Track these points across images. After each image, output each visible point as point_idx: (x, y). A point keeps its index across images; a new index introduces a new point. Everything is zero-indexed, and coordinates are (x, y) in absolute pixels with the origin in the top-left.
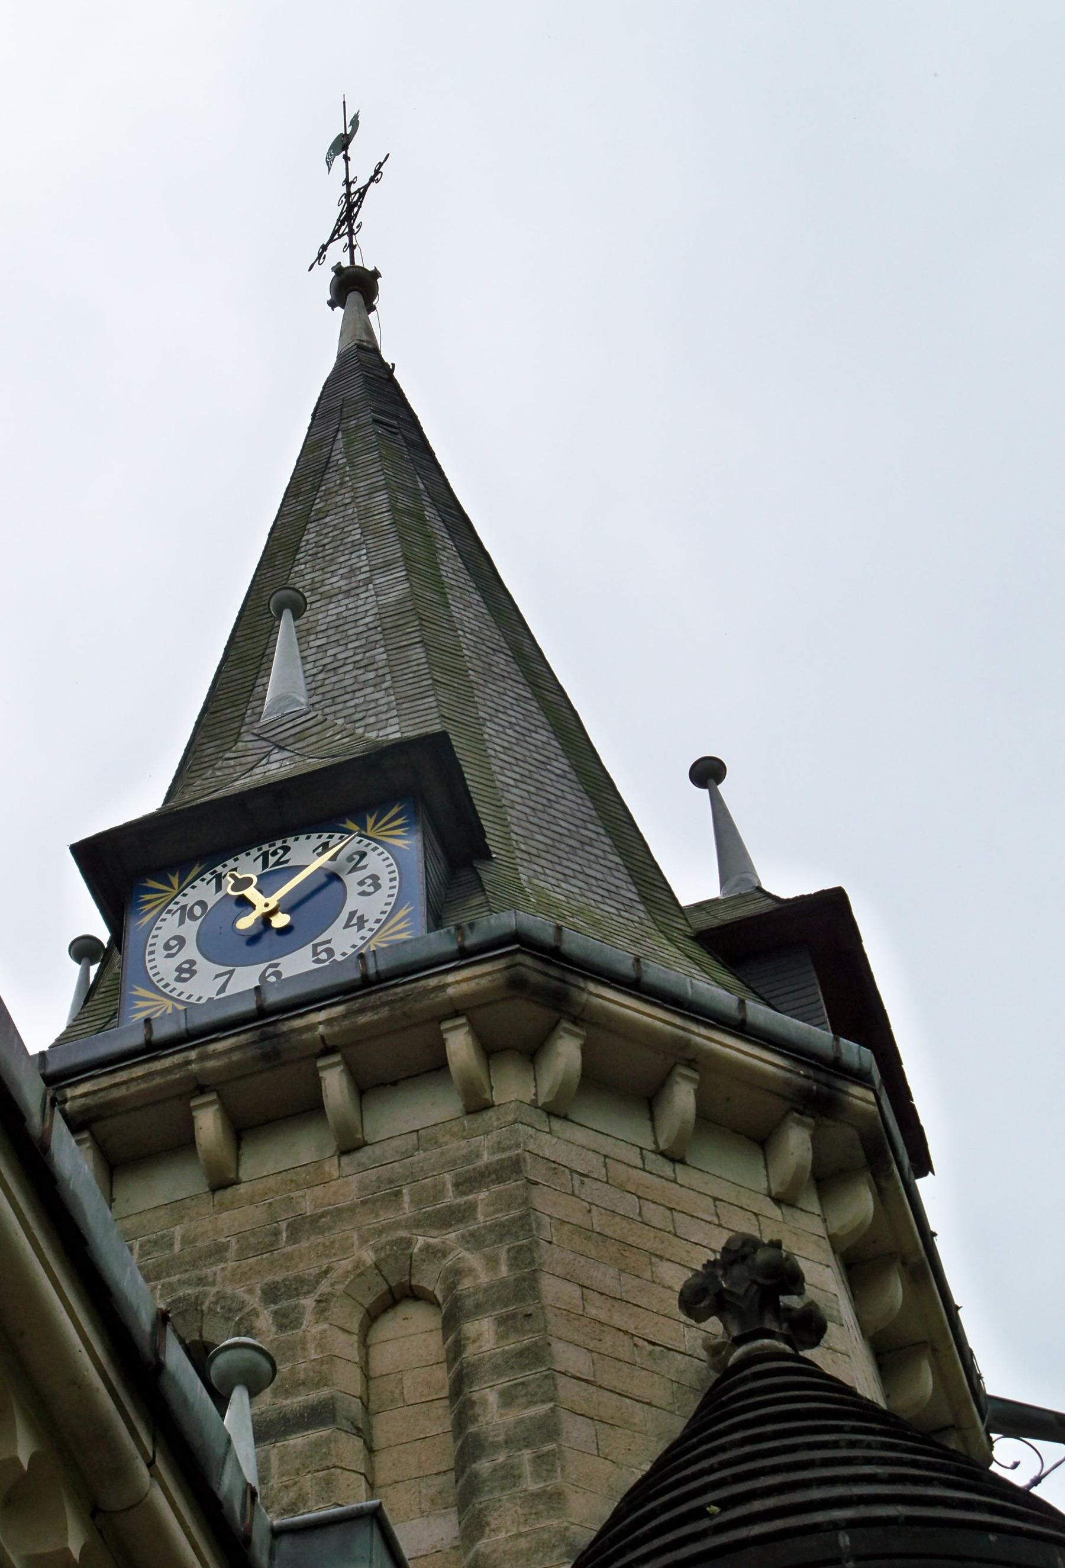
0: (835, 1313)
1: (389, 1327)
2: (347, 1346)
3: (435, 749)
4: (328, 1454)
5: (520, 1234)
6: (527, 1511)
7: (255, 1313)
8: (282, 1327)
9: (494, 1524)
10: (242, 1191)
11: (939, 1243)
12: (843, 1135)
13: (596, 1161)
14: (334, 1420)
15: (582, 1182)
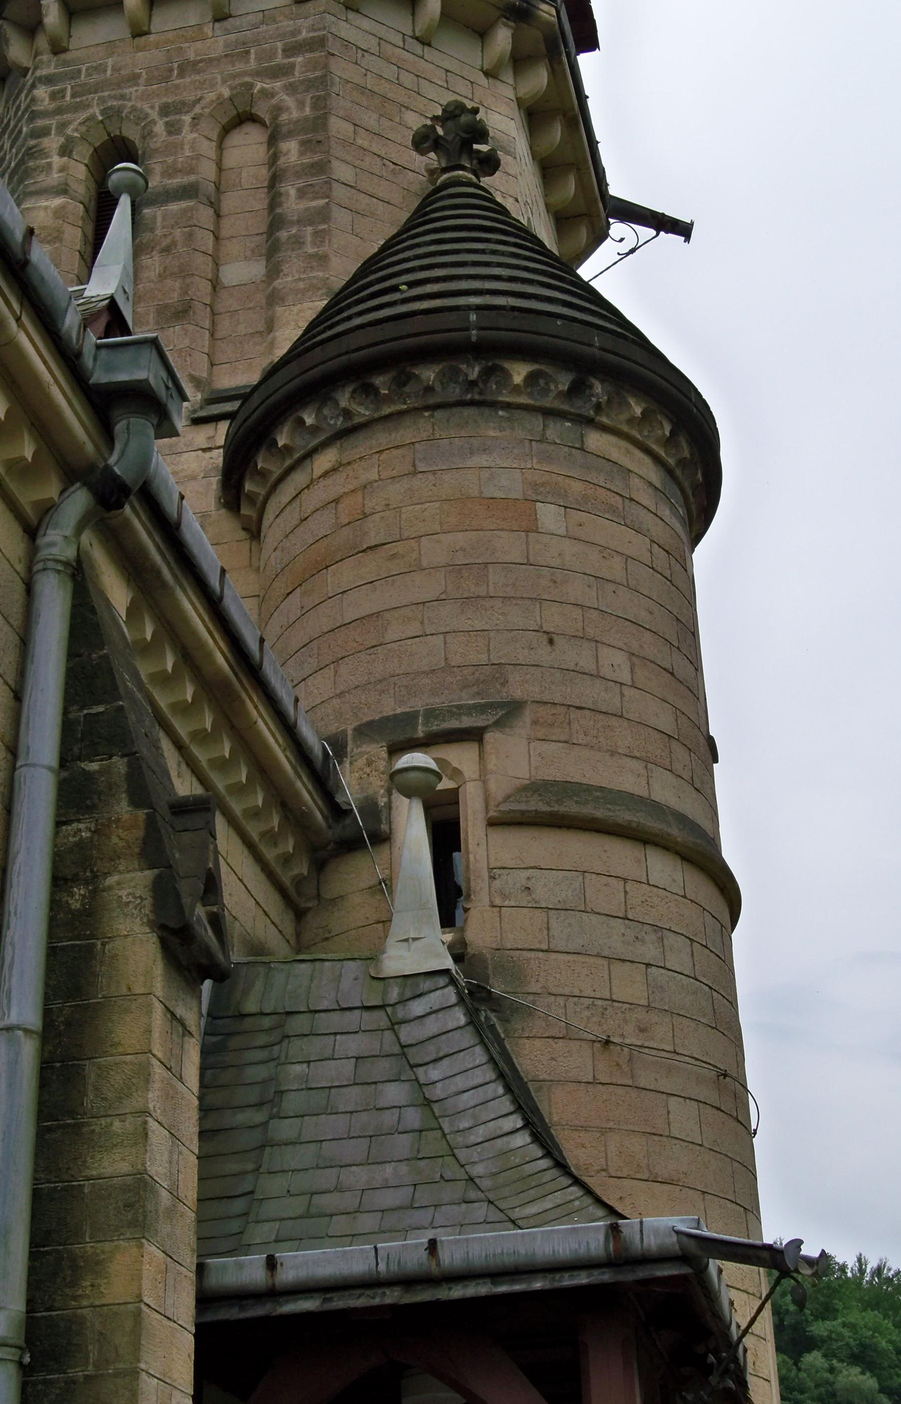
0: (512, 150)
1: (237, 138)
2: (208, 149)
4: (191, 218)
5: (319, 87)
6: (306, 265)
7: (154, 122)
8: (170, 133)
9: (286, 271)
10: (151, 39)
11: (590, 102)
12: (533, 35)
13: (374, 41)
14: (197, 196)
15: (363, 56)
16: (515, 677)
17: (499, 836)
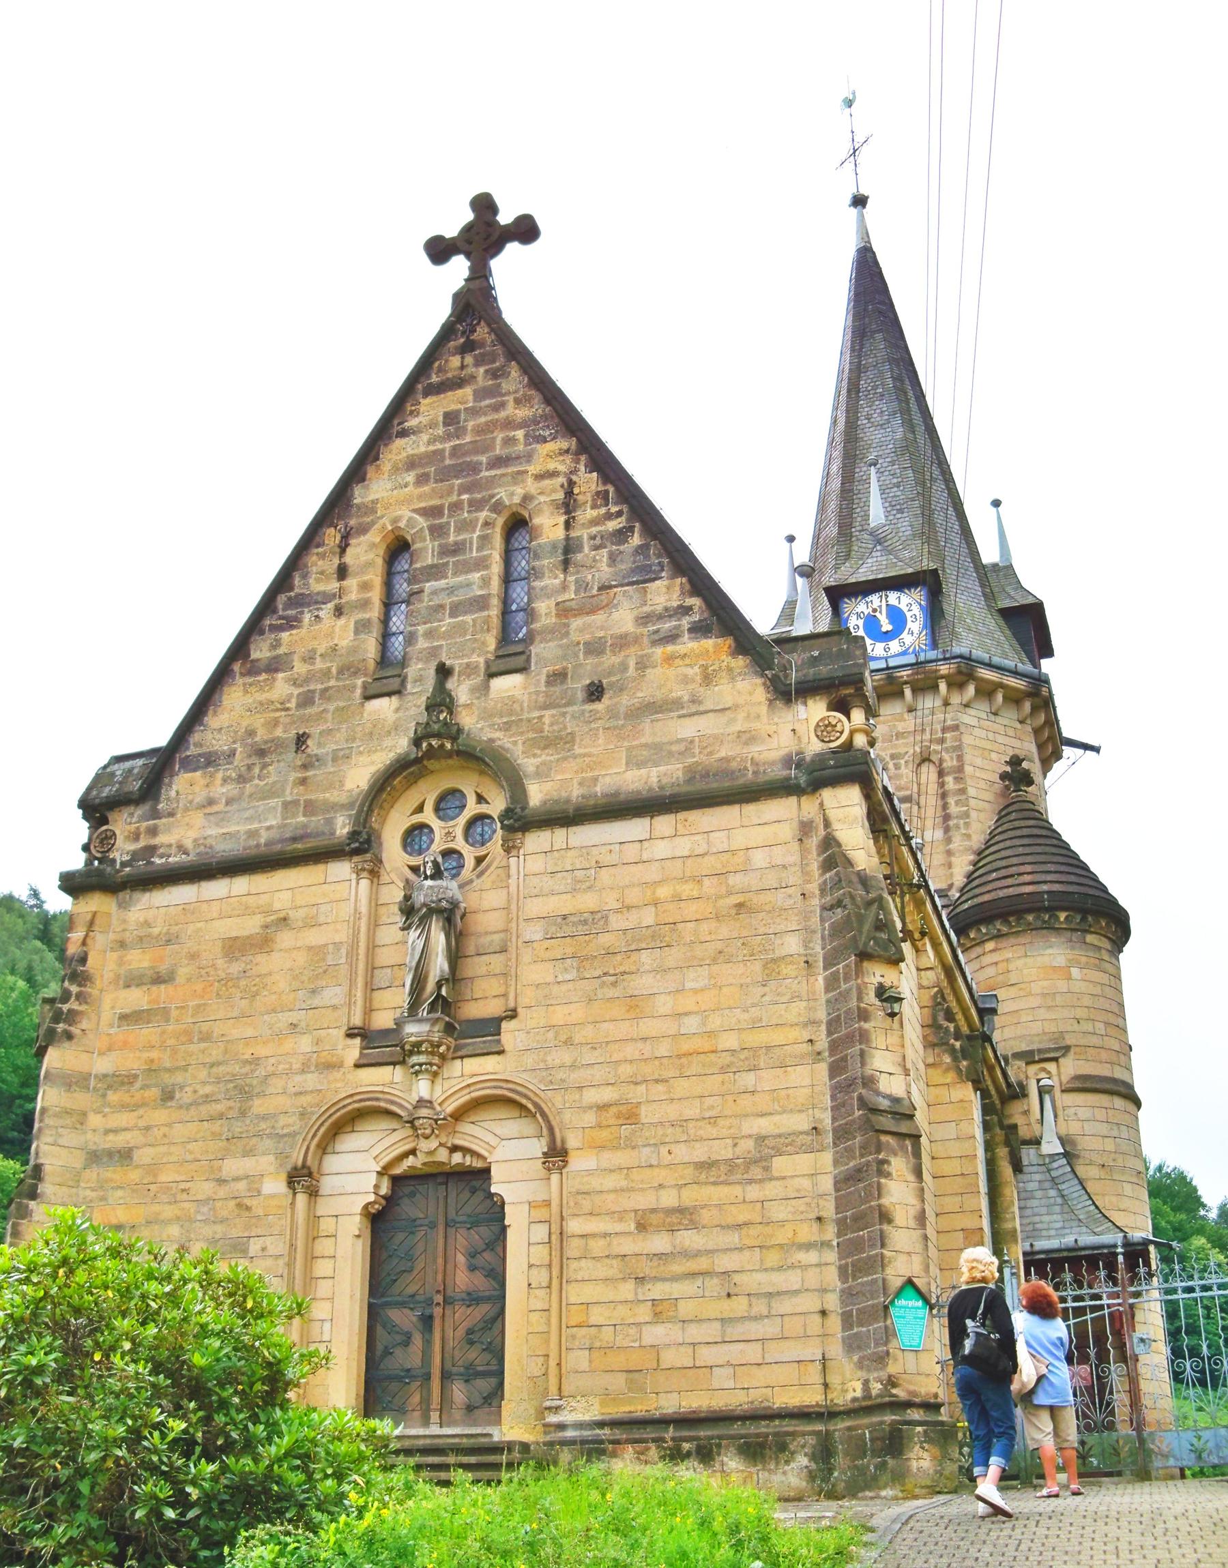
1: (924, 768)
3: (935, 572)
16: (1067, 1036)
17: (1065, 1096)
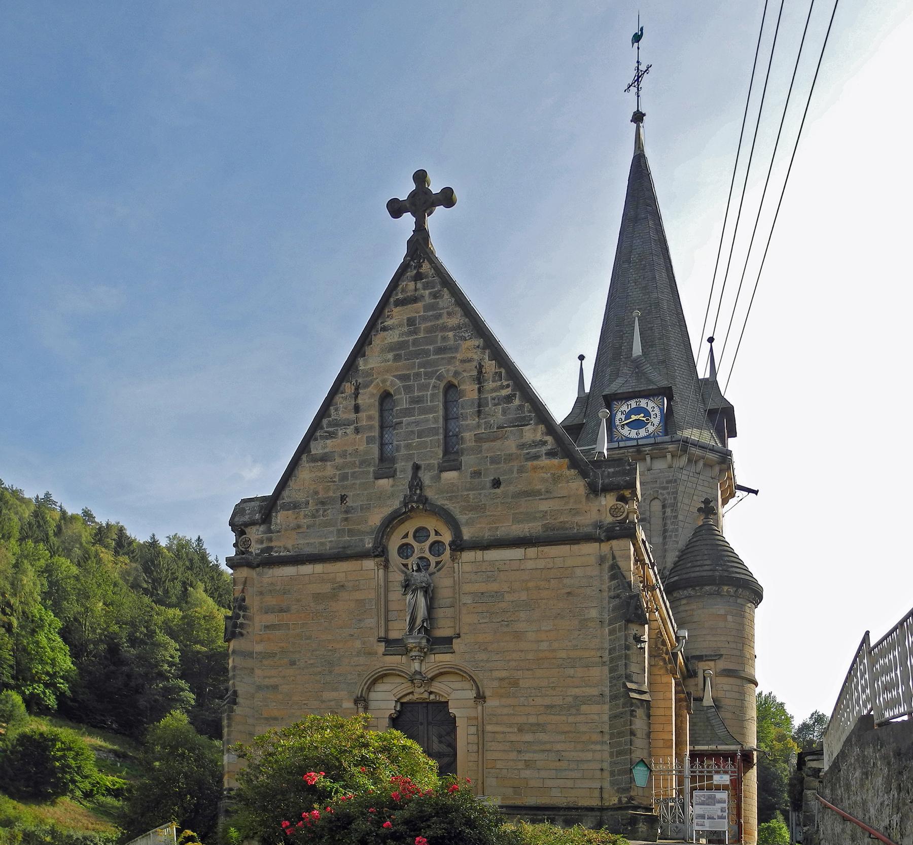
1: (654, 503)
